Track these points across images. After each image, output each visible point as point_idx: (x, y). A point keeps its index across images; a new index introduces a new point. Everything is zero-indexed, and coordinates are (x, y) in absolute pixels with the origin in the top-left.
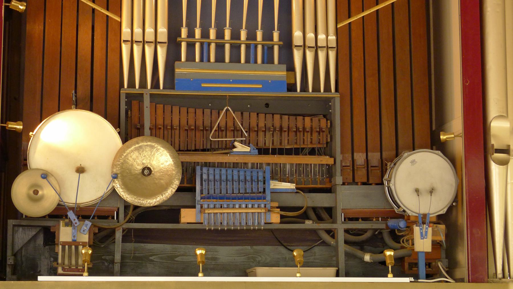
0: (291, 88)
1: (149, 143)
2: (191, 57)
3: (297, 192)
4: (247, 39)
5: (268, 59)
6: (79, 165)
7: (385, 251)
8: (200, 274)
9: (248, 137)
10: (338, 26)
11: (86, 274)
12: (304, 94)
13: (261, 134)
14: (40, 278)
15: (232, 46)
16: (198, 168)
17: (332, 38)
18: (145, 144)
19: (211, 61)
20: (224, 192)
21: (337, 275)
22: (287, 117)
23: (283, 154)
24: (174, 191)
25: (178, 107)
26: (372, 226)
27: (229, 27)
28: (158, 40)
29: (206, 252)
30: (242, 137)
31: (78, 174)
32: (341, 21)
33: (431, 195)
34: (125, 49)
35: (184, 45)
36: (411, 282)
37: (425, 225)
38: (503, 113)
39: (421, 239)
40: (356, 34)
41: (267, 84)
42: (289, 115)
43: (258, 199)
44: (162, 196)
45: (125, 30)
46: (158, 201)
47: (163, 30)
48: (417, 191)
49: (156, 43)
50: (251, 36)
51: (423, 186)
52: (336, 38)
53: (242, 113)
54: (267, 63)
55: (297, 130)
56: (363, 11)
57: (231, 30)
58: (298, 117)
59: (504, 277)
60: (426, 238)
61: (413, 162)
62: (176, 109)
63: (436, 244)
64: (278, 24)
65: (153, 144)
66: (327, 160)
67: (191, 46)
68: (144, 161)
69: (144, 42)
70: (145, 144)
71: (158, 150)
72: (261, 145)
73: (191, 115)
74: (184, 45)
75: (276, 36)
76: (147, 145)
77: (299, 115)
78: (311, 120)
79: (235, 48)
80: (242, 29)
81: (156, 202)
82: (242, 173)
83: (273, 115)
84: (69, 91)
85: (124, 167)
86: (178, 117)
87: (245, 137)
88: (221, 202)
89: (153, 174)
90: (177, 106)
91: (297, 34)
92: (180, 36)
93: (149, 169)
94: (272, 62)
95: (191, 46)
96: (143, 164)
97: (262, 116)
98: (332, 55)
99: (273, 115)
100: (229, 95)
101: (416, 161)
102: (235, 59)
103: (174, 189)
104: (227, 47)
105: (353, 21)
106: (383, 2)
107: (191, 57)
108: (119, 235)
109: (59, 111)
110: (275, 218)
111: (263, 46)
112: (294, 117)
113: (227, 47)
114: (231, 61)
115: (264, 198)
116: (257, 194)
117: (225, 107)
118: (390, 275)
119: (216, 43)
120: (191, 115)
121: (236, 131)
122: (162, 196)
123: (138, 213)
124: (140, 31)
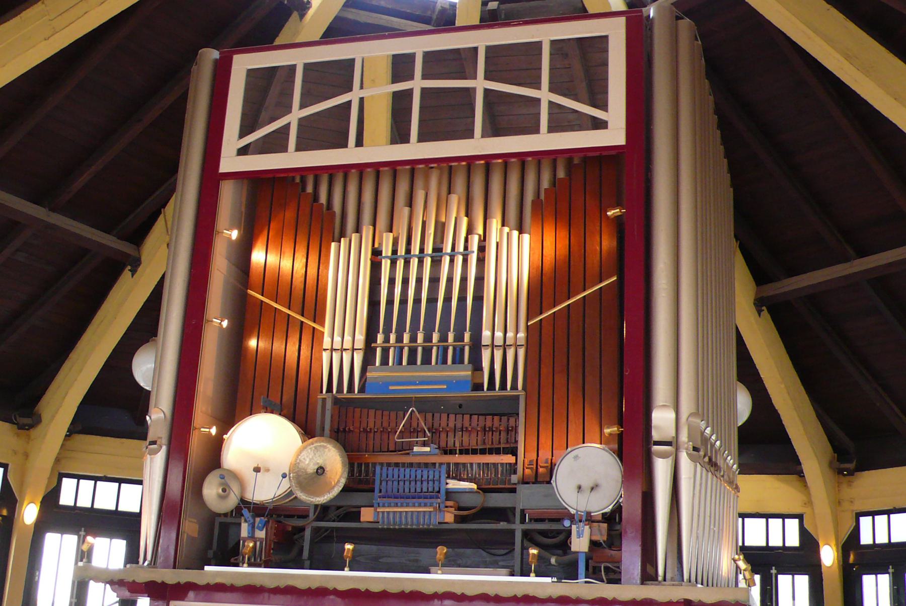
0: (478, 387)
1: (322, 444)
2: (385, 361)
3: (477, 492)
4: (439, 341)
5: (458, 359)
6: (256, 466)
7: (530, 548)
8: (346, 569)
9: (431, 437)
10: (529, 324)
11: (245, 565)
12: (503, 393)
13: (451, 435)
14: (207, 568)
15: (424, 349)
16: (378, 468)
17: (522, 335)
18: (319, 444)
19: (403, 364)
20: (401, 491)
21: (512, 574)
22: (476, 416)
23: (469, 454)
24: (341, 489)
25: (366, 410)
26: (551, 526)
27: (423, 331)
28: (334, 347)
29: (773, 566)
30: (425, 437)
31: (255, 473)
32: (532, 318)
33: (591, 492)
34: (325, 356)
35: (379, 351)
36: (553, 582)
37: (581, 523)
38: (666, 402)
39: (578, 538)
40: (547, 330)
41: (453, 384)
42: (479, 415)
43: (407, 498)
44: (330, 494)
45: (327, 341)
46: (326, 499)
47: (360, 338)
48: (579, 487)
49: (353, 350)
50: (443, 338)
51: (587, 484)
52: (526, 335)
53: (448, 415)
54: (459, 364)
55: (491, 429)
56: (554, 307)
57: (424, 333)
58: (487, 417)
59: (665, 580)
60: (582, 537)
61: (576, 457)
62: (372, 412)
63: (594, 544)
64: (384, 326)
65: (325, 444)
66: (509, 459)
67: (385, 351)
68: (318, 461)
69: (343, 350)
70: (319, 444)
71: (329, 450)
72: (443, 444)
73: (385, 418)
74: (379, 351)
75: (467, 337)
76: (320, 446)
77: (496, 415)
78: (501, 419)
79: (427, 352)
80: (450, 331)
81: (323, 500)
82: (431, 473)
83: (456, 415)
84: (275, 397)
85: (300, 467)
86: (373, 420)
87: (428, 437)
88: (396, 500)
89: (326, 473)
90: (379, 410)
91: (486, 333)
92: (376, 342)
93: (324, 470)
94: (415, 364)
95: (385, 351)
96: (318, 463)
97: (452, 417)
98: (522, 352)
99: (456, 415)
100: (415, 397)
101: (579, 456)
102: (427, 360)
103: (340, 487)
104: (420, 350)
105: (544, 318)
106: (574, 296)
107: (385, 361)
108: (308, 533)
109: (251, 415)
110: (449, 517)
111: (438, 347)
112: (484, 417)
113: (420, 350)
114: (422, 363)
115: (438, 497)
116: (431, 494)
117: (411, 408)
118: (532, 574)
119: (409, 347)
120: (385, 418)
121: (417, 432)
122: (330, 494)
123: (345, 512)
124: (340, 339)
